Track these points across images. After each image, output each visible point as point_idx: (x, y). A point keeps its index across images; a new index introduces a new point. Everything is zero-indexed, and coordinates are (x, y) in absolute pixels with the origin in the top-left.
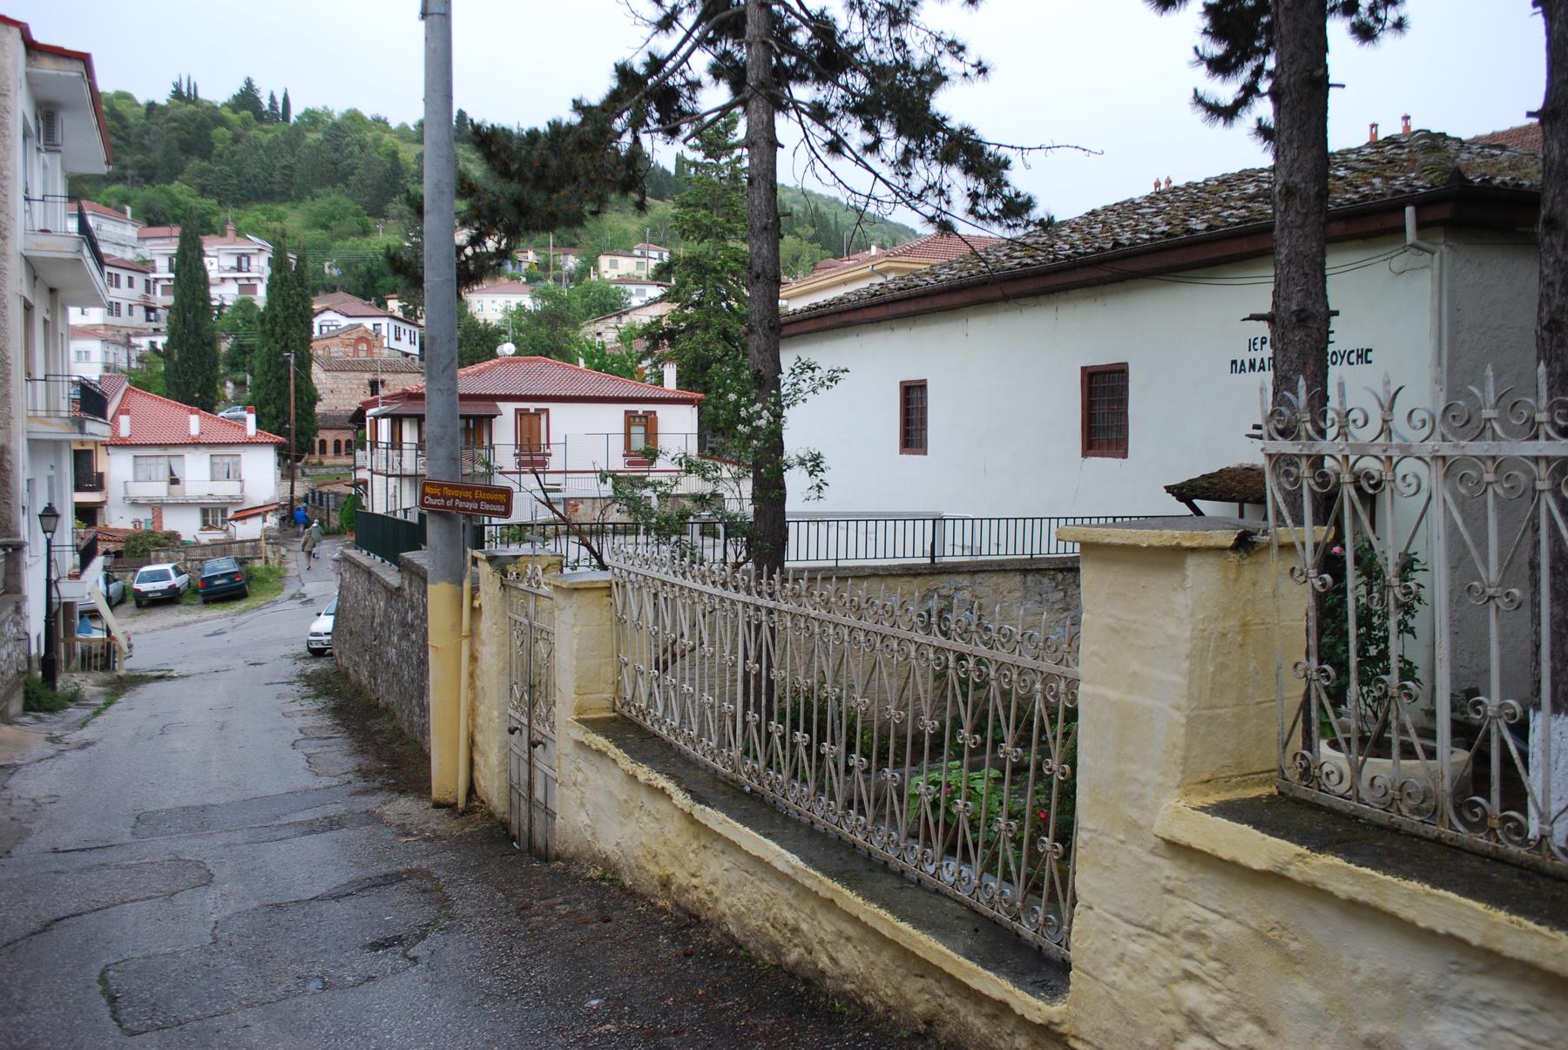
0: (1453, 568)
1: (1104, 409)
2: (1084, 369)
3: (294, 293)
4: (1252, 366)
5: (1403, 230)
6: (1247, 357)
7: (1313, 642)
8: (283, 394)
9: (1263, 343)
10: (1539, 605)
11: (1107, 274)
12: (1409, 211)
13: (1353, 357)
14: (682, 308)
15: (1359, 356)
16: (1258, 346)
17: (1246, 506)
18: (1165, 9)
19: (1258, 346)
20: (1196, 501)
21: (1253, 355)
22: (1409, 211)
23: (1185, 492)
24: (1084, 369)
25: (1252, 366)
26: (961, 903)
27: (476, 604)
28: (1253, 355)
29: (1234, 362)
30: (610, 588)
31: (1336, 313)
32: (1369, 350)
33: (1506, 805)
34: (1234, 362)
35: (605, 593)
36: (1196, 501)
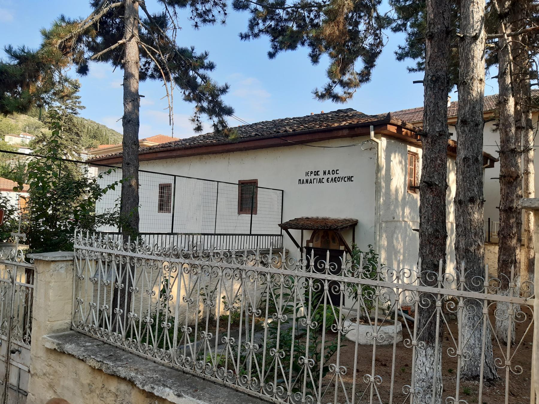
1: (247, 196)
2: (257, 180)
4: (307, 181)
9: (311, 173)
10: (100, 295)
11: (221, 149)
13: (346, 179)
15: (348, 179)
16: (309, 175)
17: (304, 231)
18: (86, 74)
19: (309, 175)
20: (289, 230)
21: (307, 177)
23: (285, 227)
24: (257, 180)
25: (307, 181)
26: (177, 370)
28: (307, 177)
29: (300, 180)
30: (73, 261)
33: (149, 344)
34: (300, 180)
35: (71, 263)
36: (289, 230)
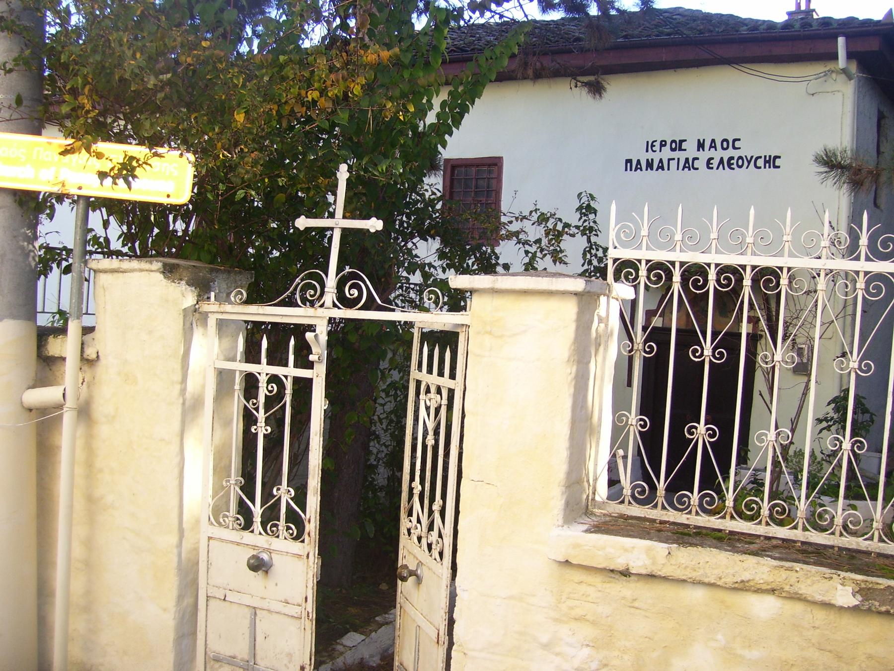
0: (732, 533)
3: (286, 63)
4: (650, 165)
5: (834, 57)
6: (644, 158)
7: (397, 633)
8: (194, 633)
12: (841, 41)
13: (760, 163)
14: (329, 23)
15: (766, 162)
16: (657, 148)
19: (657, 148)
21: (650, 155)
22: (841, 41)
27: (90, 353)
28: (650, 155)
31: (830, 163)
32: (776, 157)
34: (629, 161)
